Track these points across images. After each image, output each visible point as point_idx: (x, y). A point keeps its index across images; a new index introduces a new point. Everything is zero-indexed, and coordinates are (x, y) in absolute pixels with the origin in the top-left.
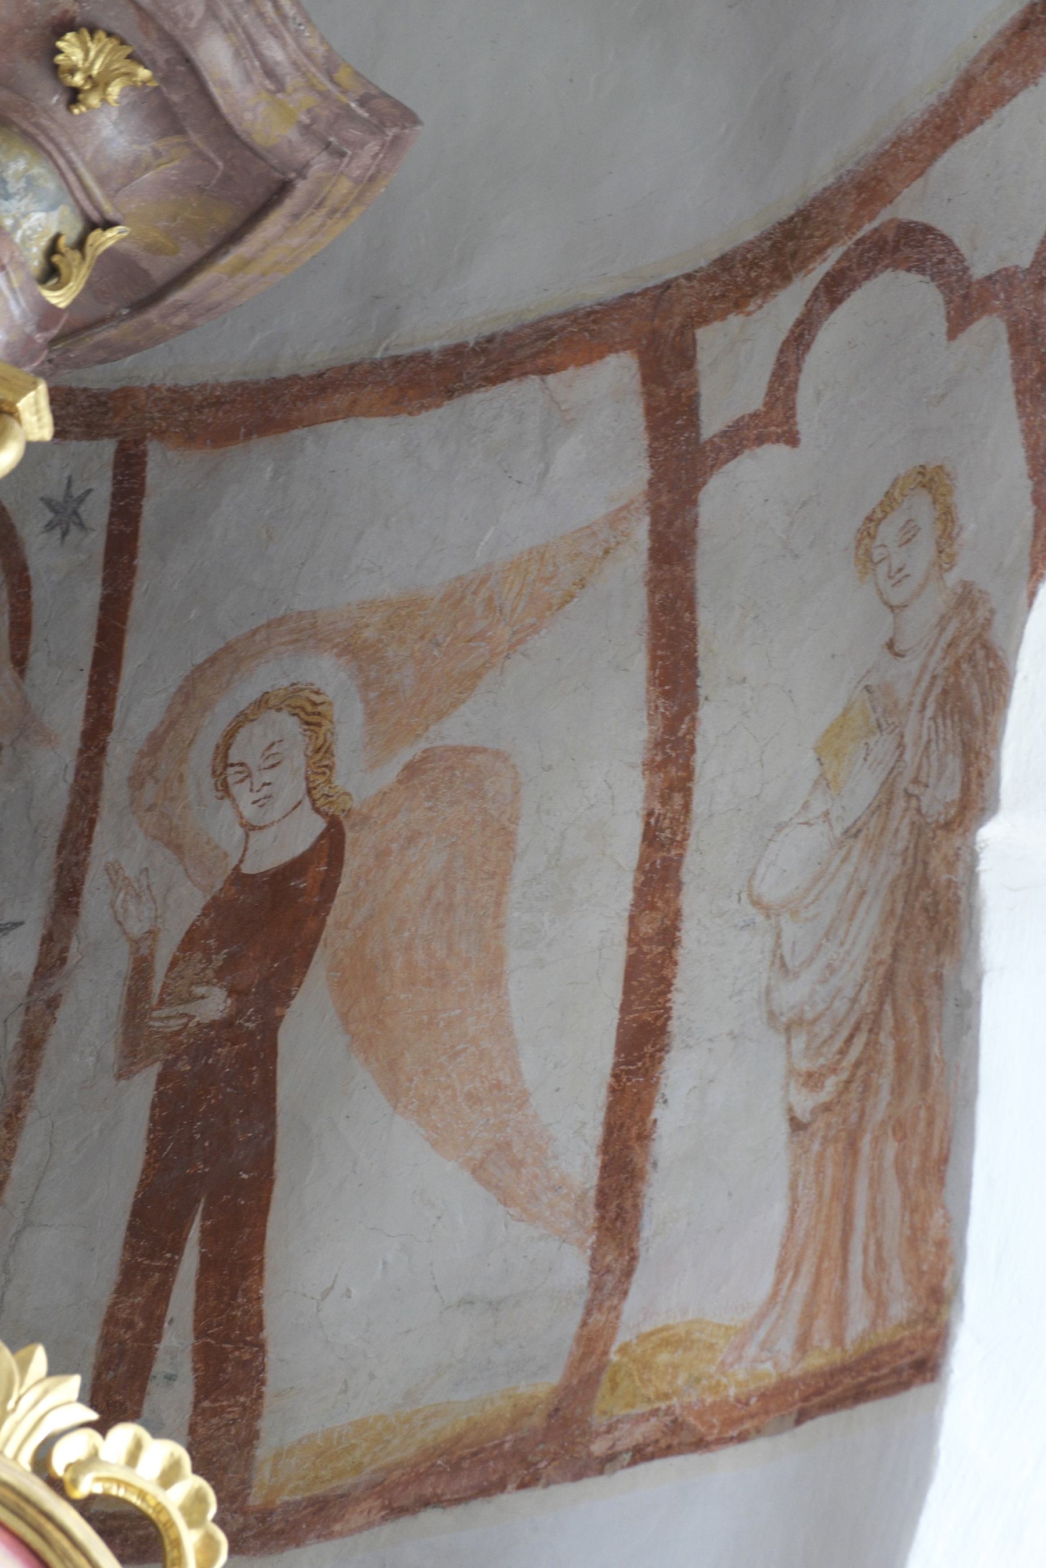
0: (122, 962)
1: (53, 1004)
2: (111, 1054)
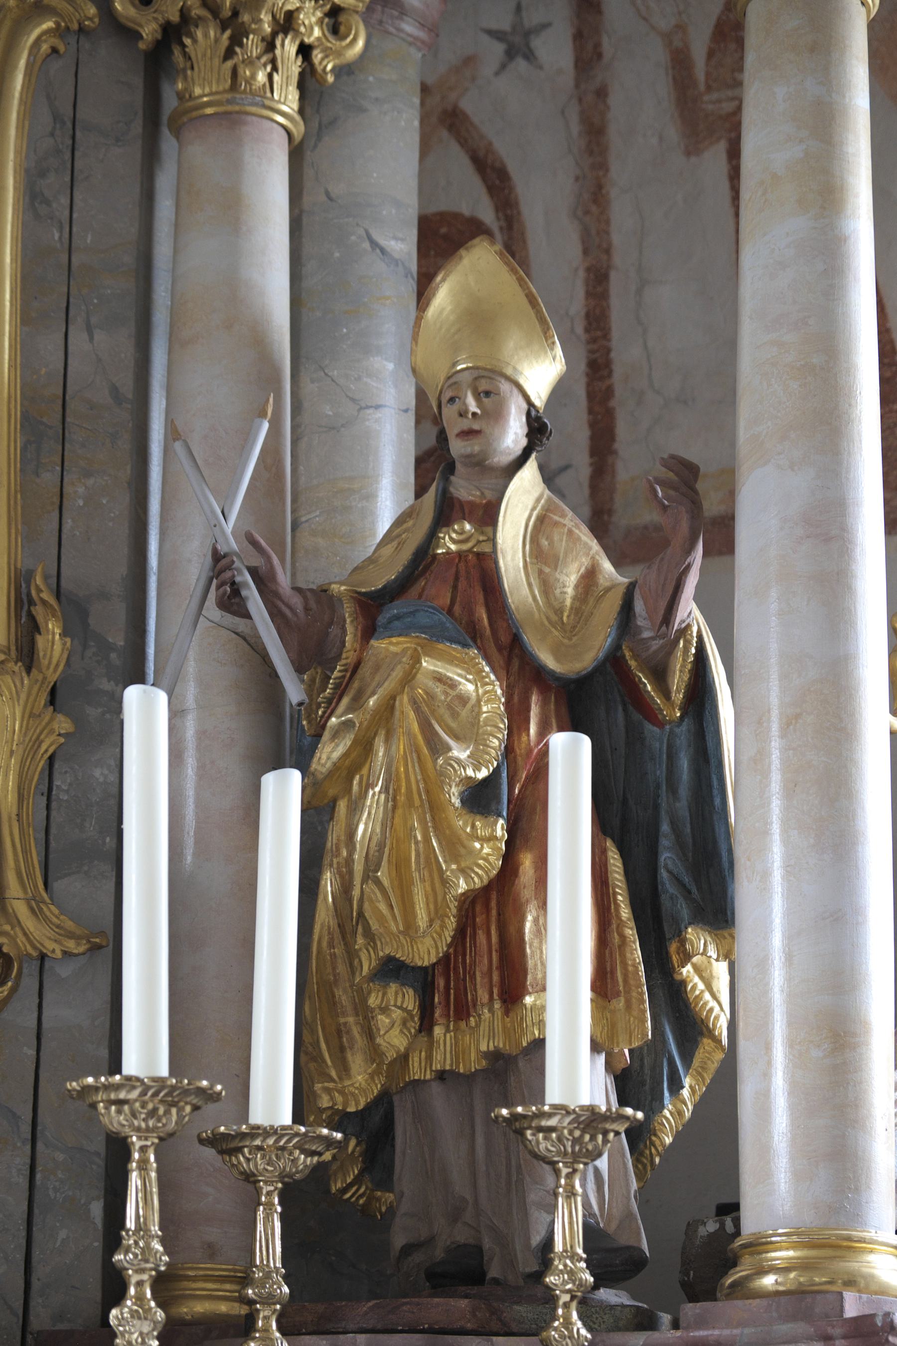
0: (658, 54)
1: (602, 93)
2: (673, 134)
